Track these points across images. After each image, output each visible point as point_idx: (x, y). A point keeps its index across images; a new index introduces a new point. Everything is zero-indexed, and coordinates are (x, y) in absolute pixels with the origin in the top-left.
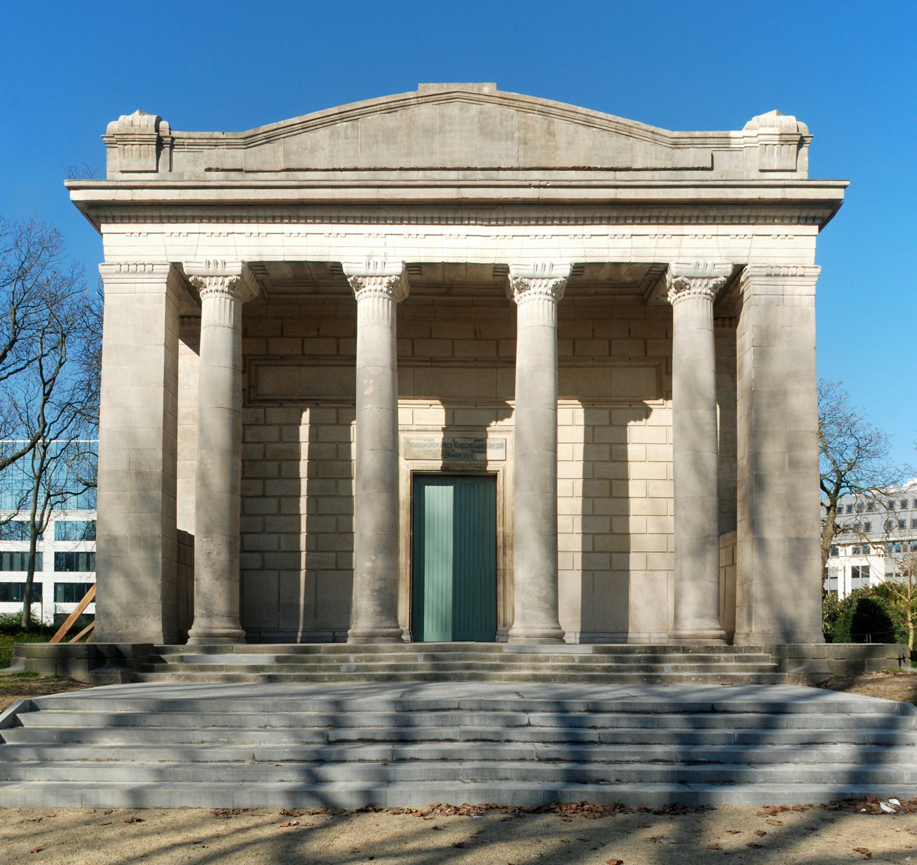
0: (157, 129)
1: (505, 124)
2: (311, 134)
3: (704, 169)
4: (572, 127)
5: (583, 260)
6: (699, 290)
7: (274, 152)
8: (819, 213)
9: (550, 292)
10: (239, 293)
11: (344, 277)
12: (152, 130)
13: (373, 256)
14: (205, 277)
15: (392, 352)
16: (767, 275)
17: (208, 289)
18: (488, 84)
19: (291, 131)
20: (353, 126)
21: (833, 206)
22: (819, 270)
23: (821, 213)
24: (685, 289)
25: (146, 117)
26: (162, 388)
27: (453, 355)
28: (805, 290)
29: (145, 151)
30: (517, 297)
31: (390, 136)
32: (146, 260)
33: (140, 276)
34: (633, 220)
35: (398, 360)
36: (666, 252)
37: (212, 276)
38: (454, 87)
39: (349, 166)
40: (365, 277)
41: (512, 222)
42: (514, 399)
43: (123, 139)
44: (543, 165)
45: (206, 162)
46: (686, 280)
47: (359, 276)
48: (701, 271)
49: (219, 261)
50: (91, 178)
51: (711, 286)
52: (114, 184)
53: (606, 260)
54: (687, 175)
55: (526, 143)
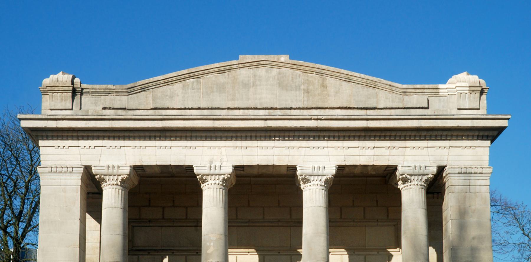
0: (73, 83)
1: (295, 80)
2: (170, 87)
3: (423, 108)
4: (338, 82)
5: (343, 163)
6: (417, 183)
7: (146, 97)
8: (491, 134)
9: (323, 184)
10: (127, 185)
11: (195, 176)
12: (69, 84)
13: (214, 162)
14: (106, 175)
15: (225, 224)
16: (459, 173)
17: (108, 183)
18: (284, 56)
19: (157, 84)
21: (500, 130)
22: (492, 170)
23: (491, 133)
24: (408, 182)
25: (66, 75)
26: (78, 249)
27: (264, 218)
28: (483, 182)
29: (65, 96)
30: (302, 186)
31: (221, 88)
32: (68, 164)
33: (64, 175)
34: (375, 138)
35: (229, 222)
37: (111, 175)
38: (262, 57)
39: (195, 106)
40: (208, 175)
41: (299, 138)
42: (302, 249)
43: (52, 89)
44: (320, 106)
45: (102, 104)
46: (408, 176)
47: (204, 175)
48: (417, 171)
49: (115, 166)
50: (32, 113)
51: (424, 180)
52: (46, 117)
53: (358, 163)
54: (413, 112)
55: (308, 92)
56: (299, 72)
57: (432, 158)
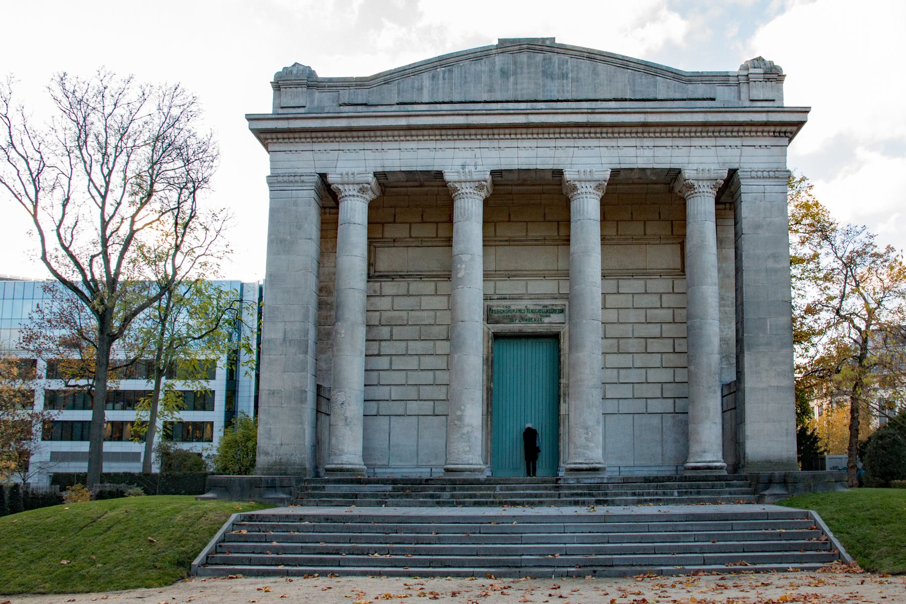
5: (618, 166)
20: (449, 70)
36: (680, 160)
39: (447, 100)
53: (635, 166)
56: (566, 57)
57: (715, 160)
